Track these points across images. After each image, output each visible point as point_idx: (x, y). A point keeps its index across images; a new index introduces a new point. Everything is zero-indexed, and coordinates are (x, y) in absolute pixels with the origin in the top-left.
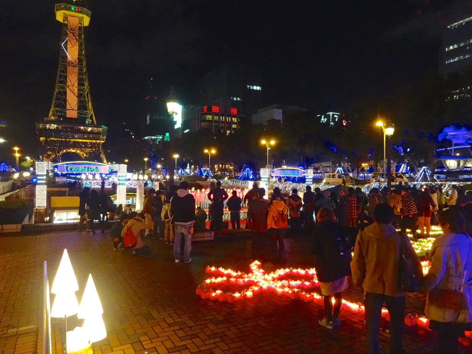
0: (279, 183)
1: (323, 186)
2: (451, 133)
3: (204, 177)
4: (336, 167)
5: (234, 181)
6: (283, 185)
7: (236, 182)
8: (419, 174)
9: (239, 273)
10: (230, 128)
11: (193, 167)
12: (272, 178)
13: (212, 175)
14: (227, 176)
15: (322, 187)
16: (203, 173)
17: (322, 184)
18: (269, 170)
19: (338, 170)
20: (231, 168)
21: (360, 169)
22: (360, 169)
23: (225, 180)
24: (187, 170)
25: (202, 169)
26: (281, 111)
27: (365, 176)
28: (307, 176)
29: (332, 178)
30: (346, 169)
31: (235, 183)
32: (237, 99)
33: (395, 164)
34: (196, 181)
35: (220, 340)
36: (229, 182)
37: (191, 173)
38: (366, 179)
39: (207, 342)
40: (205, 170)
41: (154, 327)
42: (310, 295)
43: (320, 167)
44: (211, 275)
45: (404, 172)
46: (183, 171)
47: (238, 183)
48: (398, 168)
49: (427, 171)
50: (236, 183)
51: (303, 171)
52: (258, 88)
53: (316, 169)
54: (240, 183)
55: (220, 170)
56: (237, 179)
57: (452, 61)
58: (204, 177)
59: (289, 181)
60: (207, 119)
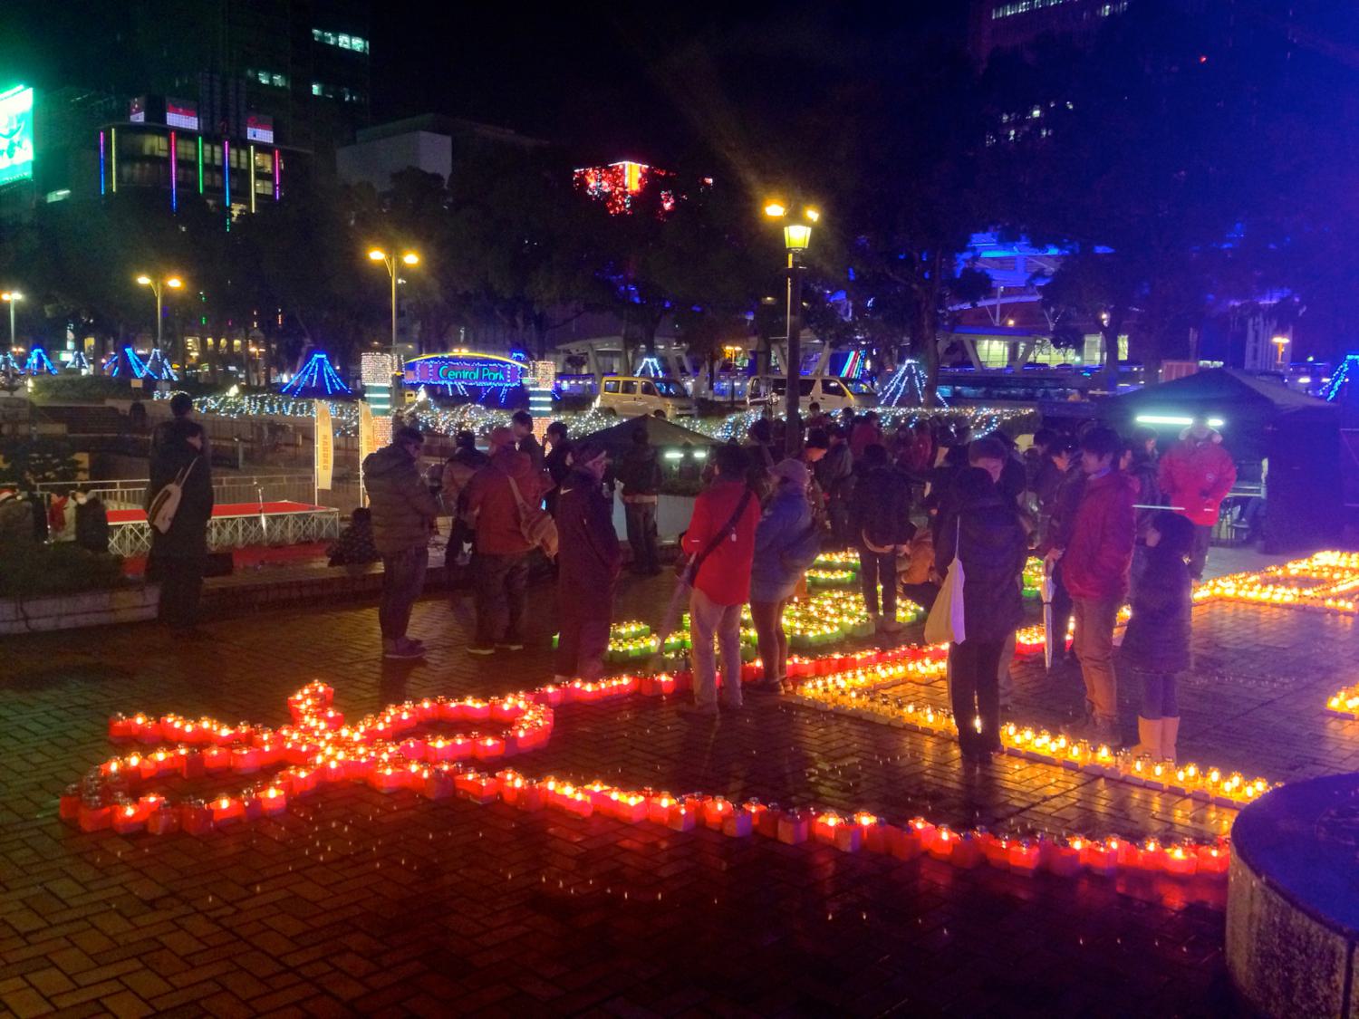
0: (438, 410)
1: (591, 419)
2: (990, 252)
3: (137, 384)
4: (638, 356)
5: (262, 400)
6: (454, 416)
7: (271, 405)
8: (894, 381)
9: (244, 729)
10: (241, 194)
11: (90, 342)
12: (413, 393)
13: (175, 379)
14: (237, 381)
15: (587, 423)
16: (137, 371)
17: (589, 414)
18: (396, 361)
19: (644, 364)
20: (253, 350)
21: (717, 366)
22: (717, 366)
23: (227, 398)
24: (67, 357)
25: (128, 350)
26: (448, 140)
27: (733, 386)
28: (533, 386)
29: (623, 392)
30: (672, 363)
31: (268, 409)
32: (271, 80)
33: (827, 352)
34: (102, 400)
35: (140, 965)
36: (243, 405)
37: (81, 365)
38: (736, 399)
39: (83, 980)
40: (144, 358)
41: (41, 974)
42: (491, 780)
43: (587, 354)
44: (132, 742)
45: (855, 375)
46: (49, 358)
47: (280, 407)
48: (837, 363)
49: (917, 374)
50: (272, 409)
51: (520, 365)
52: (358, 44)
53: (572, 366)
54: (290, 408)
55: (206, 355)
56: (280, 392)
57: (1009, 13)
58: (136, 384)
59: (474, 403)
60: (147, 151)
